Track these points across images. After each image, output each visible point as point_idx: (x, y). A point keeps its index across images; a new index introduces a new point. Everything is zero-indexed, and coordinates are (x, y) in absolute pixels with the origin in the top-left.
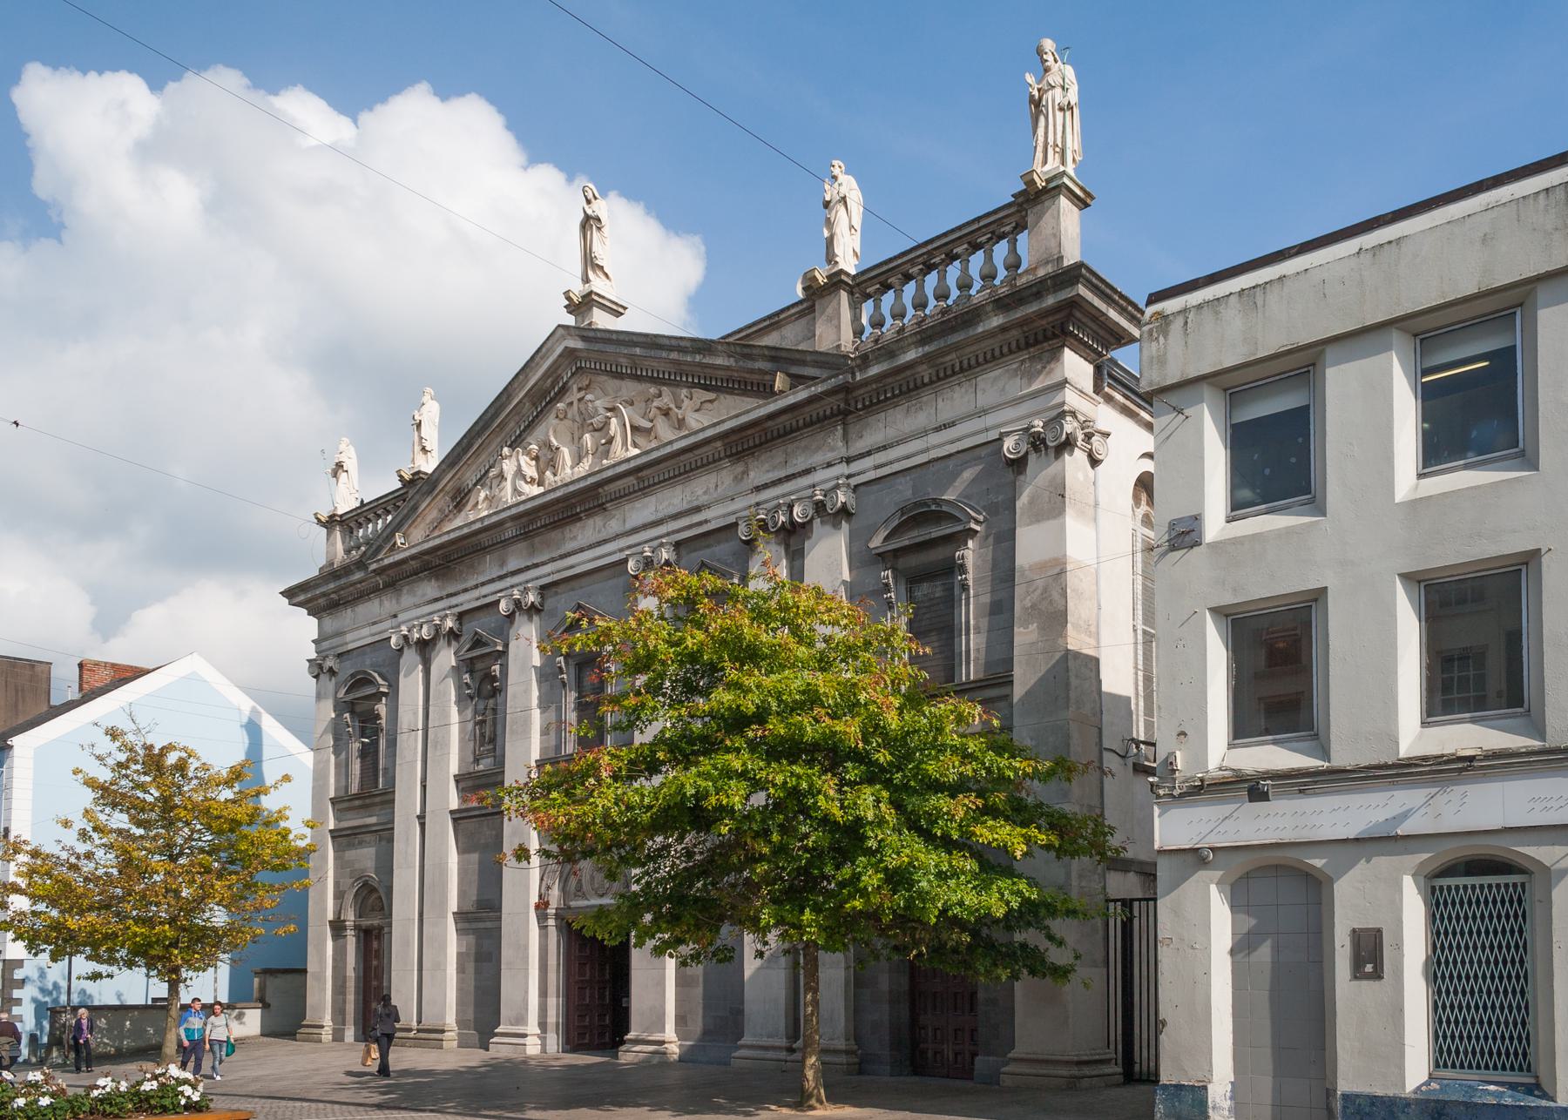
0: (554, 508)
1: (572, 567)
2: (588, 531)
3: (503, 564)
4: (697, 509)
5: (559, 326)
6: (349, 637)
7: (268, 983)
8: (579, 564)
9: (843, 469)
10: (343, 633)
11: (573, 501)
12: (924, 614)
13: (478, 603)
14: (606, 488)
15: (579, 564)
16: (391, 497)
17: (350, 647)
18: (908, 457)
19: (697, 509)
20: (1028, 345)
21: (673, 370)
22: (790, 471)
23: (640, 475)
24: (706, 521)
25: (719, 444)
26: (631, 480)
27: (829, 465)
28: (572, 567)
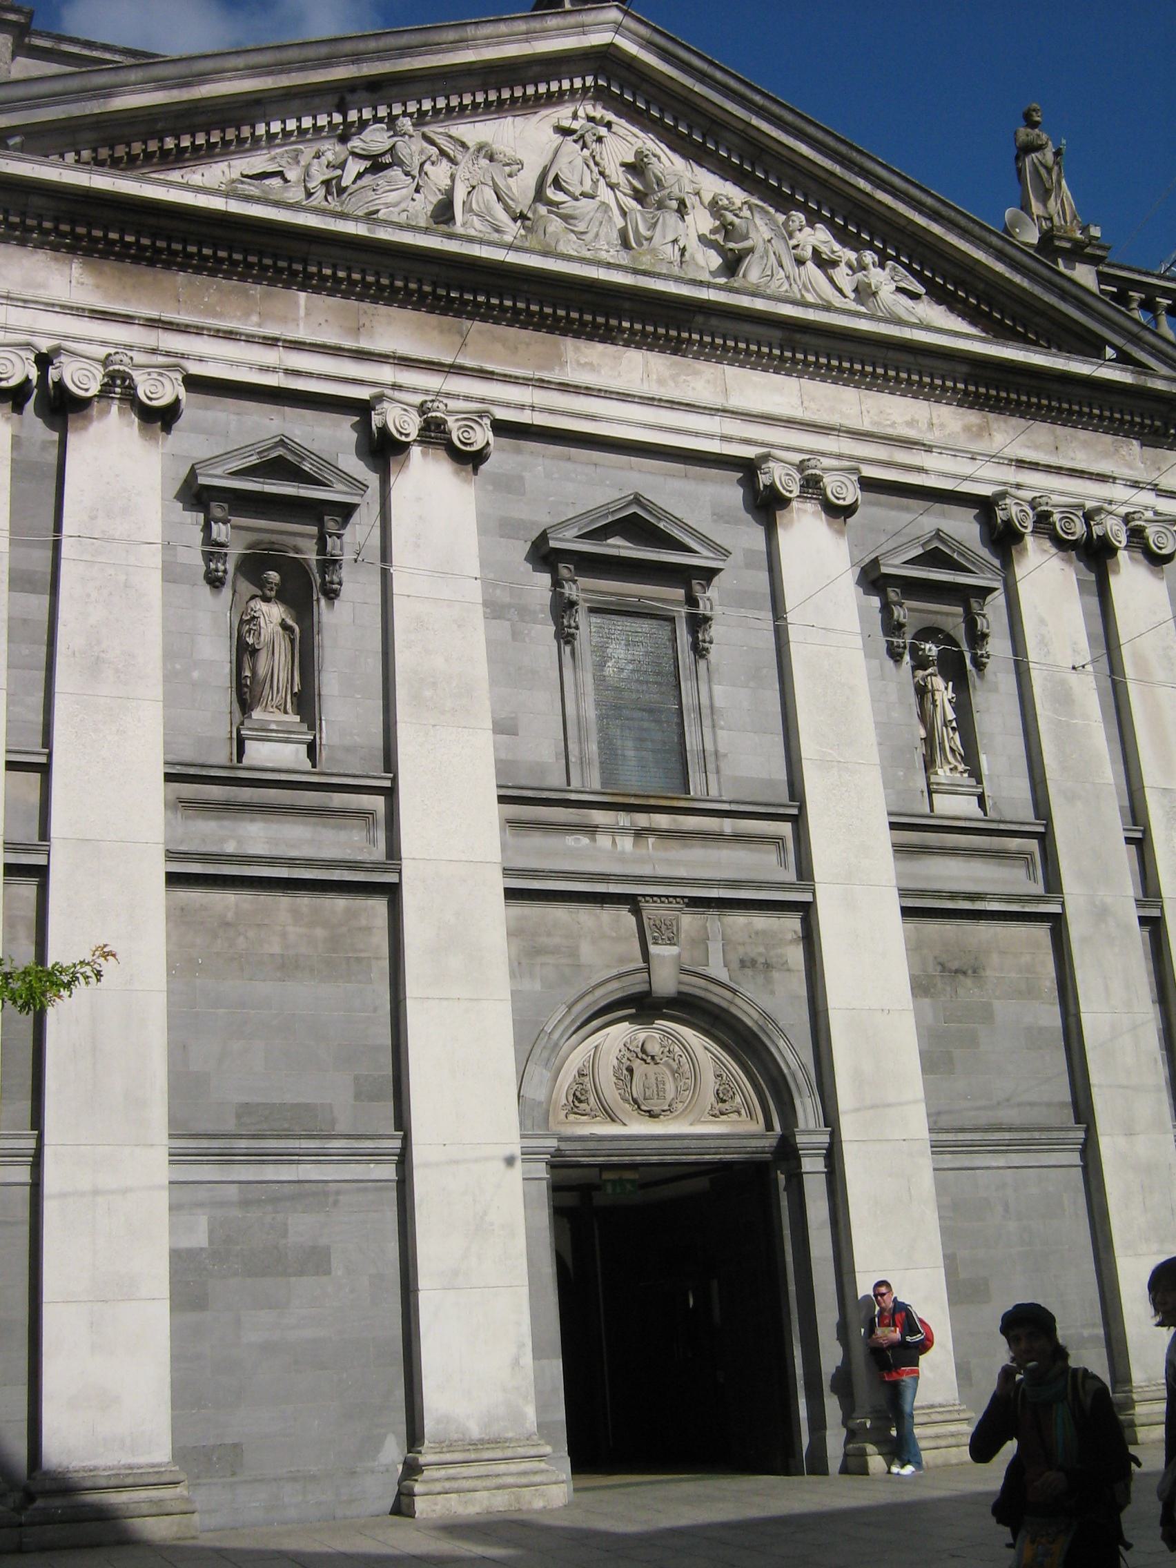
3: (357, 331)
8: (609, 420)
15: (609, 420)
24: (921, 470)
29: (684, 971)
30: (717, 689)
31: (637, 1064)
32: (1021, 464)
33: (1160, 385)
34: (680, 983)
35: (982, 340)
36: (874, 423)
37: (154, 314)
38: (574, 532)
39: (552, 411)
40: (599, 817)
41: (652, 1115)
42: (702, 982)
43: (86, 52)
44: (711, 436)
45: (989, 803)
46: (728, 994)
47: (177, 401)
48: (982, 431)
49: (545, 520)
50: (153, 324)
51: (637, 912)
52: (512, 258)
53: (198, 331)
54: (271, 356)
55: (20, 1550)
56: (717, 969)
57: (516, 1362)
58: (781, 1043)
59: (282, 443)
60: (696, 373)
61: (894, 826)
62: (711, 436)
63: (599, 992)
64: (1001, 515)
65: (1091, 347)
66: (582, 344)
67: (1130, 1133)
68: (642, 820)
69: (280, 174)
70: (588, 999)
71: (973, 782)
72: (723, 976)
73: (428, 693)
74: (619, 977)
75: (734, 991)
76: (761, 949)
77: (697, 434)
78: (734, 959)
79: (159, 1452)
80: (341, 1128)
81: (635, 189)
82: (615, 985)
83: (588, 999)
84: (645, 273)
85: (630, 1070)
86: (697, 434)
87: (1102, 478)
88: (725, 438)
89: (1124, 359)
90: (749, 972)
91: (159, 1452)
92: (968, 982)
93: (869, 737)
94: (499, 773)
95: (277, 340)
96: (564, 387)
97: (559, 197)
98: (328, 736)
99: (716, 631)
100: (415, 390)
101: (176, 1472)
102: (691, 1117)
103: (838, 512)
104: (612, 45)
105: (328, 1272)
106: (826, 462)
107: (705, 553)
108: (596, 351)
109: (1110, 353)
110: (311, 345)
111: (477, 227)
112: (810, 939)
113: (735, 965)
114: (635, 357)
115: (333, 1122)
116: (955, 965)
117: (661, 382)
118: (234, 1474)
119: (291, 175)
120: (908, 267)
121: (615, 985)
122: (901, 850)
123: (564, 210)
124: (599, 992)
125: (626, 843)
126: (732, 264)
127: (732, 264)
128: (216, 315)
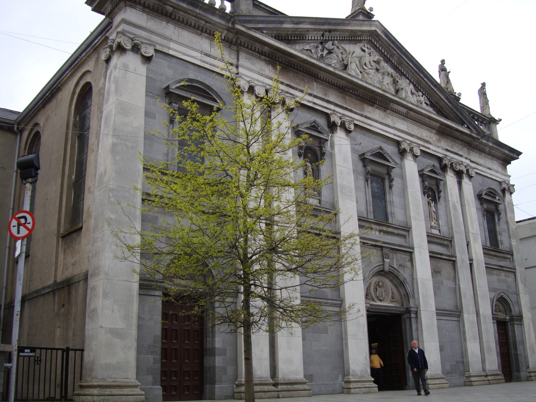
0: (368, 93)
1: (371, 125)
2: (376, 113)
3: (326, 95)
4: (427, 142)
5: (378, 21)
6: (172, 45)
7: (336, 250)
8: (374, 127)
9: (468, 162)
10: (171, 40)
11: (379, 98)
12: (201, 289)
13: (310, 105)
14: (395, 105)
15: (374, 127)
16: (267, 8)
17: (171, 52)
18: (482, 171)
19: (427, 142)
20: (268, 57)
21: (350, 36)
22: (451, 150)
23: (409, 111)
24: (429, 148)
25: (438, 125)
26: (404, 110)
27: (466, 158)
28: (371, 125)
29: (390, 266)
30: (394, 197)
31: (378, 288)
32: (447, 150)
33: (474, 135)
34: (389, 269)
35: (434, 114)
36: (421, 136)
37: (288, 83)
38: (369, 154)
39: (363, 122)
40: (373, 226)
41: (381, 301)
42: (393, 269)
43: (265, 8)
44: (392, 134)
45: (441, 232)
46: (398, 273)
47: (152, 56)
48: (439, 141)
49: (365, 150)
50: (287, 85)
51: (382, 250)
52: (360, 82)
53: (296, 89)
54: (311, 99)
55: (279, 397)
56: (395, 266)
57: (366, 358)
58: (407, 285)
59: (315, 122)
60: (389, 117)
61: (359, 220)
62: (392, 134)
63: (375, 269)
64: (444, 162)
65: (462, 124)
66: (368, 106)
67: (469, 314)
68: (381, 228)
69: (310, 50)
70: (373, 271)
71: (438, 226)
72: (396, 267)
73: (344, 190)
74: (378, 266)
75: (399, 272)
76: (403, 262)
77: (389, 133)
78: (398, 264)
79: (300, 376)
80: (329, 297)
81: (377, 68)
82: (378, 268)
83: (373, 271)
84: (385, 91)
85: (377, 289)
86: (389, 133)
87: (461, 156)
88: (395, 135)
89: (468, 127)
90: (401, 267)
91: (300, 376)
92: (439, 274)
93: (422, 213)
94: (358, 213)
95: (312, 94)
96: (366, 117)
97: (366, 68)
98: (323, 199)
99: (394, 183)
100: (340, 113)
101: (305, 380)
102: (388, 302)
103: (415, 156)
104: (376, 31)
105: (328, 333)
106: (347, 118)
107: (393, 163)
108: (370, 108)
109: (466, 126)
110: (319, 97)
111: (353, 73)
112: (411, 260)
113: (398, 265)
114: (377, 111)
115: (327, 296)
116: (436, 270)
117: (382, 118)
118: (312, 382)
119: (313, 51)
120: (427, 97)
121: (378, 268)
122: (429, 242)
123: (366, 71)
124: (375, 269)
125: (377, 233)
126: (397, 91)
127: (397, 91)
128: (299, 85)
